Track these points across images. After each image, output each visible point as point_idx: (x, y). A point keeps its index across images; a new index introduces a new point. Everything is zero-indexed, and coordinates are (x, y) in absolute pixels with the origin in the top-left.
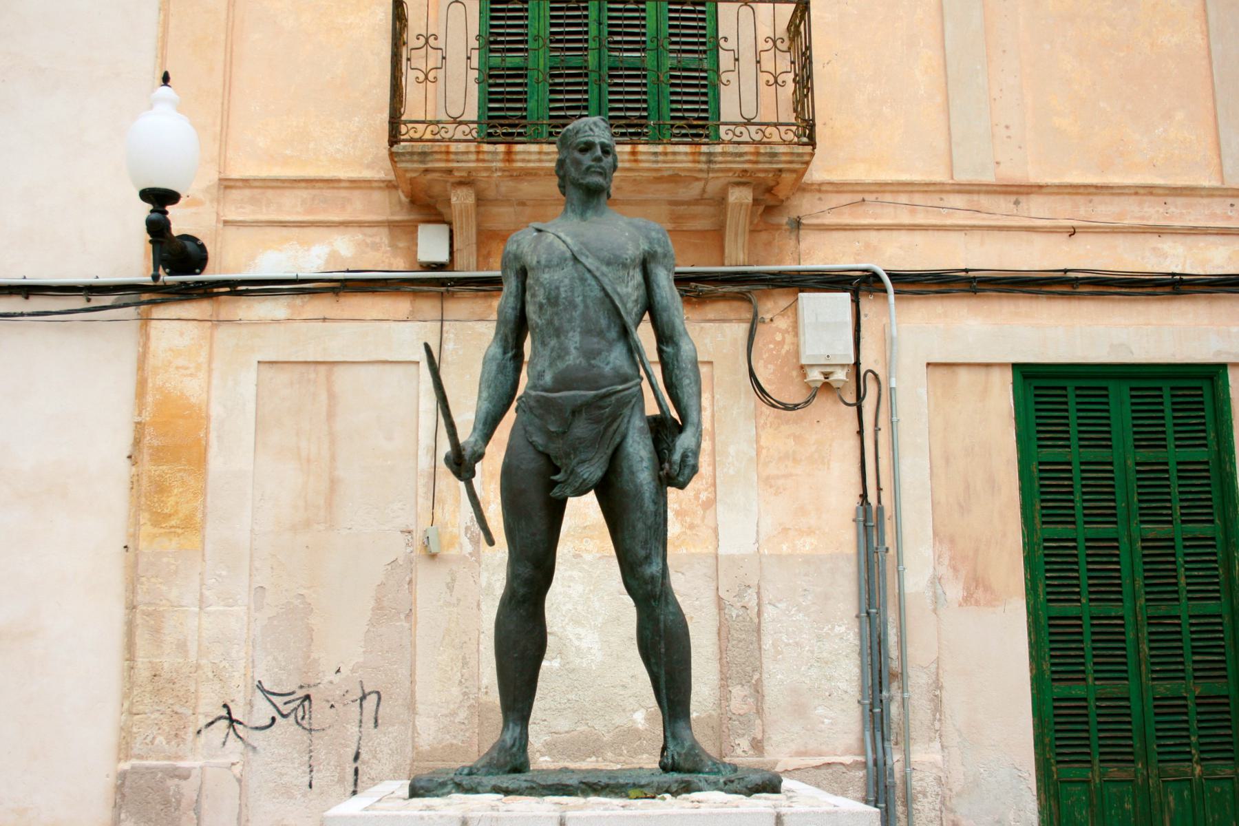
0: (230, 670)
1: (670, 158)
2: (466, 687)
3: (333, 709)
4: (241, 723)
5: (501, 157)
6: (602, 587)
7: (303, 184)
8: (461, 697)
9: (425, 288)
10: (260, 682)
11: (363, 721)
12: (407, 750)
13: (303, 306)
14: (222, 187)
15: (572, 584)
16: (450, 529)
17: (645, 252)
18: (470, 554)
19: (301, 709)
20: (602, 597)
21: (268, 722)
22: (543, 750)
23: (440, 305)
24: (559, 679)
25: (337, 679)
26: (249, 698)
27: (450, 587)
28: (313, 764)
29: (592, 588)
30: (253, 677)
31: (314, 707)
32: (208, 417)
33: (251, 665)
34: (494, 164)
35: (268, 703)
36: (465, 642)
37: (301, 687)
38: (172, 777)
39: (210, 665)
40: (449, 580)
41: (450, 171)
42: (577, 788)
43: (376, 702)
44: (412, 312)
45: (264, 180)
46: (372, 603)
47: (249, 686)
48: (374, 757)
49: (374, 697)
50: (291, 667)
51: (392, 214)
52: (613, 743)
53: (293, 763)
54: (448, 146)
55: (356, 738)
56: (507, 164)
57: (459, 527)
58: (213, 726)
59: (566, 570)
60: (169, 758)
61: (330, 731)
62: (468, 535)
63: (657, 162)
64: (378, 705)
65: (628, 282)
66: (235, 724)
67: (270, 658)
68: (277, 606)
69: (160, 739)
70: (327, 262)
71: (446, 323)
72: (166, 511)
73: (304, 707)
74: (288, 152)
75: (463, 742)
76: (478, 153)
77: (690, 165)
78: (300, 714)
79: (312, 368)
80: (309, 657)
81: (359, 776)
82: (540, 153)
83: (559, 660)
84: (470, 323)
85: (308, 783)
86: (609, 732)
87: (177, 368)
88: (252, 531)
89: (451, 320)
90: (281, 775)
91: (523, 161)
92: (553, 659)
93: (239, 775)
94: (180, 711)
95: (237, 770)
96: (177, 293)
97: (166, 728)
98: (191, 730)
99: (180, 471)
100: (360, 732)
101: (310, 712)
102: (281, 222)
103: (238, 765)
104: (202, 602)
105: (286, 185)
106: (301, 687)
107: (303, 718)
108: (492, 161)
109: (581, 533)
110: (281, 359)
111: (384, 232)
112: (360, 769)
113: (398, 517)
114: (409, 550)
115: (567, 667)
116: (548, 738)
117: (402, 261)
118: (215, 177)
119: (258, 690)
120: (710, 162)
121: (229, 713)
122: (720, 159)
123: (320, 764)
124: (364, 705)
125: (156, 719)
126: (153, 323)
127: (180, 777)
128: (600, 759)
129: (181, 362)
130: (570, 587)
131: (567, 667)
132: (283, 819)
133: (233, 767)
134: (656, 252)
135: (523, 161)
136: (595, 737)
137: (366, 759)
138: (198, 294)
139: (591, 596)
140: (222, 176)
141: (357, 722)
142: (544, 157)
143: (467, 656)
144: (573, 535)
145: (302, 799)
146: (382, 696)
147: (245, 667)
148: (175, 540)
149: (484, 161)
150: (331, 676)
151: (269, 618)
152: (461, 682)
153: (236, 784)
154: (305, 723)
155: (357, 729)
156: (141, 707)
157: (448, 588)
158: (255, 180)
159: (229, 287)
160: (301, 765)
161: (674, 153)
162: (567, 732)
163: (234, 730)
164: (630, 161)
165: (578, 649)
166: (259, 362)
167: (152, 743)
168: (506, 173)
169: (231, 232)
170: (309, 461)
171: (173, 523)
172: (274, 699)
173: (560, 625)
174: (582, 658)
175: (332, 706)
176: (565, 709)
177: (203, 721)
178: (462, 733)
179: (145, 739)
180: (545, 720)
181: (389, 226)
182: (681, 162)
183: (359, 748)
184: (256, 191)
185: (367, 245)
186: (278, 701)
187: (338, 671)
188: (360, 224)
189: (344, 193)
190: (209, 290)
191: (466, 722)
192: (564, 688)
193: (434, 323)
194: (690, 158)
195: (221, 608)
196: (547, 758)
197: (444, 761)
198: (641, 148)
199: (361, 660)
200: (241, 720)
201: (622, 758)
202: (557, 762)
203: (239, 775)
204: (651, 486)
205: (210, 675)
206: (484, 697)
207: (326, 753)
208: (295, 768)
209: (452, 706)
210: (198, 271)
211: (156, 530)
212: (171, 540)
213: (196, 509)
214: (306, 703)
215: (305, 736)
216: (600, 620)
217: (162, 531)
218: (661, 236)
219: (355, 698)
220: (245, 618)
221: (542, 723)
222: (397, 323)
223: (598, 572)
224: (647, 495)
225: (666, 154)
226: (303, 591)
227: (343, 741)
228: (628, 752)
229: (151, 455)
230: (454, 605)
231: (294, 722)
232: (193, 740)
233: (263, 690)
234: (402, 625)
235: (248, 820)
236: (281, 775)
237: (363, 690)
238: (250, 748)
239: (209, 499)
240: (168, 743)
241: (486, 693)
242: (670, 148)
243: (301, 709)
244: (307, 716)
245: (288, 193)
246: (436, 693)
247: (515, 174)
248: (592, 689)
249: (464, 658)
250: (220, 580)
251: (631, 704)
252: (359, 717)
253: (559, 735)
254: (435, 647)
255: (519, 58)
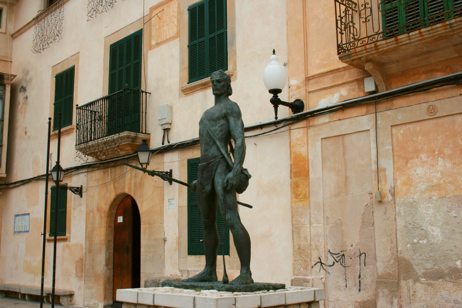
0: (320, 246)
1: (435, 30)
2: (393, 251)
3: (351, 260)
4: (324, 264)
5: (374, 49)
6: (440, 210)
7: (330, 73)
8: (391, 255)
9: (369, 102)
10: (329, 250)
11: (361, 264)
12: (375, 275)
13: (333, 116)
14: (307, 80)
15: (429, 209)
16: (384, 191)
17: (224, 114)
18: (391, 200)
19: (342, 259)
20: (441, 214)
21: (332, 264)
22: (422, 276)
23: (375, 107)
24: (426, 247)
25: (351, 248)
26: (326, 255)
27: (385, 213)
28: (347, 279)
29: (437, 210)
30: (327, 248)
31: (346, 259)
32: (308, 160)
33: (326, 244)
34: (373, 52)
35: (332, 257)
36: (391, 234)
37: (341, 251)
38: (304, 282)
39: (314, 244)
40: (384, 210)
41: (360, 59)
42: (190, 287)
43: (364, 257)
44: (367, 112)
45: (318, 75)
46: (361, 221)
47: (326, 251)
48: (365, 277)
49: (363, 255)
50: (338, 244)
51: (358, 76)
52: (449, 274)
53: (341, 278)
54: (356, 50)
55: (359, 270)
56: (377, 51)
57: (387, 190)
58: (316, 265)
59: (426, 204)
60: (304, 275)
61: (351, 267)
62: (390, 193)
63: (430, 34)
64: (365, 258)
65: (216, 125)
66: (322, 264)
67: (332, 241)
68: (332, 223)
69: (302, 269)
70: (339, 99)
71: (377, 114)
72: (299, 193)
73: (342, 258)
74: (325, 63)
75: (393, 272)
76: (366, 49)
77: (444, 31)
78: (342, 261)
79: (337, 138)
80: (343, 241)
81: (361, 284)
82: (386, 43)
83: (426, 240)
84: (385, 112)
85: (345, 286)
86: (447, 269)
87: (299, 145)
88: (323, 198)
89: (379, 112)
90: (337, 282)
91: (382, 48)
92: (424, 239)
93: (324, 282)
94: (306, 260)
95: (323, 280)
96: (295, 120)
97: (303, 265)
98: (310, 266)
99: (301, 179)
100: (360, 267)
101: (344, 260)
102: (324, 88)
103: (324, 279)
104: (310, 223)
105: (325, 74)
106: (341, 251)
107: (343, 262)
108: (372, 51)
109: (431, 188)
110: (327, 136)
111: (356, 83)
112: (361, 281)
113: (367, 188)
114: (372, 200)
115: (429, 242)
116: (424, 271)
117: (362, 93)
118: (303, 77)
119: (329, 253)
120: (451, 27)
121: (321, 261)
122: (455, 25)
123: (348, 279)
124: (361, 258)
125: (300, 262)
126: (291, 131)
127: (306, 282)
128: (444, 280)
129: (299, 143)
130: (428, 210)
131: (429, 242)
132: (338, 298)
133: (322, 279)
134: (228, 112)
135: (382, 48)
136: (441, 271)
137: (363, 277)
138: (302, 119)
139: (437, 214)
140: (307, 76)
141: (359, 264)
142: (388, 44)
143: (392, 239)
144: (428, 190)
145: (344, 291)
146: (366, 254)
147: (324, 245)
148: (302, 203)
149: (368, 52)
150: (350, 248)
151: (331, 228)
152: (391, 249)
153: (323, 285)
154: (343, 264)
155: (359, 266)
156: (296, 259)
157: (385, 214)
158: (315, 75)
159: (310, 115)
160: (343, 279)
161: (436, 28)
162: (431, 269)
163: (322, 266)
164: (420, 36)
165: (433, 235)
166: (322, 139)
167: (300, 270)
168: (379, 54)
169: (311, 95)
170: (338, 171)
171: (301, 197)
172: (334, 255)
173: (425, 226)
174: (434, 239)
175: (351, 258)
176: (429, 260)
177: (314, 263)
178: (392, 269)
179: (298, 269)
180: (422, 264)
181: (357, 81)
182: (440, 31)
183: (360, 273)
184: (317, 79)
185: (351, 90)
186: (335, 256)
187: (352, 246)
188: (348, 83)
189: (342, 73)
190: (305, 117)
191: (393, 264)
192: (428, 251)
193: (373, 114)
194: (443, 28)
195: (316, 225)
196: (424, 279)
197: (386, 279)
198: (423, 30)
199: (359, 241)
200: (324, 263)
201: (453, 280)
202: (427, 280)
203: (324, 282)
204: (221, 191)
205: (315, 248)
206: (400, 255)
207: (350, 275)
208: (341, 280)
209: (388, 258)
210: (301, 111)
211: (297, 200)
212: (301, 203)
213: (307, 191)
214: (343, 257)
215: (342, 268)
216: (440, 223)
217: (298, 200)
218: (230, 106)
219: (358, 255)
220: (323, 228)
221: (421, 265)
222: (361, 117)
223: (439, 204)
224: (220, 194)
225: (433, 29)
226: (340, 218)
227: (355, 271)
228: (455, 277)
229: (294, 175)
230: (387, 220)
231: (340, 264)
232: (311, 270)
233: (330, 253)
234: (371, 228)
235: (328, 298)
236: (337, 282)
237: (360, 252)
238: (327, 273)
239: (310, 188)
240: (304, 270)
241: (400, 253)
242: (434, 27)
243: (342, 259)
244: (344, 262)
245: (326, 77)
246: (383, 253)
247: (381, 53)
248: (439, 251)
249: (391, 240)
250: (315, 215)
251: (455, 258)
252: (359, 262)
253: (427, 270)
254: (381, 236)
255: (389, 6)
